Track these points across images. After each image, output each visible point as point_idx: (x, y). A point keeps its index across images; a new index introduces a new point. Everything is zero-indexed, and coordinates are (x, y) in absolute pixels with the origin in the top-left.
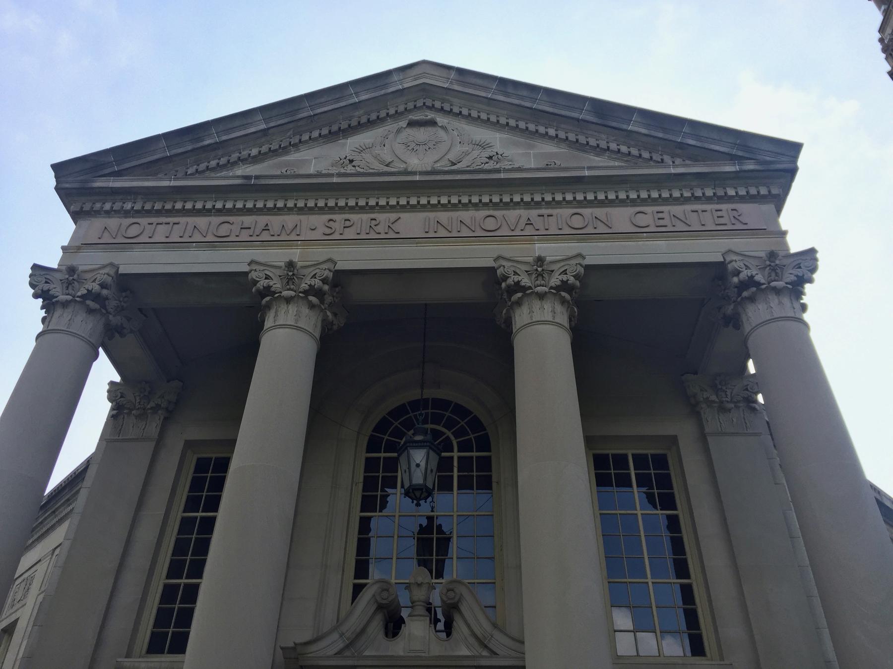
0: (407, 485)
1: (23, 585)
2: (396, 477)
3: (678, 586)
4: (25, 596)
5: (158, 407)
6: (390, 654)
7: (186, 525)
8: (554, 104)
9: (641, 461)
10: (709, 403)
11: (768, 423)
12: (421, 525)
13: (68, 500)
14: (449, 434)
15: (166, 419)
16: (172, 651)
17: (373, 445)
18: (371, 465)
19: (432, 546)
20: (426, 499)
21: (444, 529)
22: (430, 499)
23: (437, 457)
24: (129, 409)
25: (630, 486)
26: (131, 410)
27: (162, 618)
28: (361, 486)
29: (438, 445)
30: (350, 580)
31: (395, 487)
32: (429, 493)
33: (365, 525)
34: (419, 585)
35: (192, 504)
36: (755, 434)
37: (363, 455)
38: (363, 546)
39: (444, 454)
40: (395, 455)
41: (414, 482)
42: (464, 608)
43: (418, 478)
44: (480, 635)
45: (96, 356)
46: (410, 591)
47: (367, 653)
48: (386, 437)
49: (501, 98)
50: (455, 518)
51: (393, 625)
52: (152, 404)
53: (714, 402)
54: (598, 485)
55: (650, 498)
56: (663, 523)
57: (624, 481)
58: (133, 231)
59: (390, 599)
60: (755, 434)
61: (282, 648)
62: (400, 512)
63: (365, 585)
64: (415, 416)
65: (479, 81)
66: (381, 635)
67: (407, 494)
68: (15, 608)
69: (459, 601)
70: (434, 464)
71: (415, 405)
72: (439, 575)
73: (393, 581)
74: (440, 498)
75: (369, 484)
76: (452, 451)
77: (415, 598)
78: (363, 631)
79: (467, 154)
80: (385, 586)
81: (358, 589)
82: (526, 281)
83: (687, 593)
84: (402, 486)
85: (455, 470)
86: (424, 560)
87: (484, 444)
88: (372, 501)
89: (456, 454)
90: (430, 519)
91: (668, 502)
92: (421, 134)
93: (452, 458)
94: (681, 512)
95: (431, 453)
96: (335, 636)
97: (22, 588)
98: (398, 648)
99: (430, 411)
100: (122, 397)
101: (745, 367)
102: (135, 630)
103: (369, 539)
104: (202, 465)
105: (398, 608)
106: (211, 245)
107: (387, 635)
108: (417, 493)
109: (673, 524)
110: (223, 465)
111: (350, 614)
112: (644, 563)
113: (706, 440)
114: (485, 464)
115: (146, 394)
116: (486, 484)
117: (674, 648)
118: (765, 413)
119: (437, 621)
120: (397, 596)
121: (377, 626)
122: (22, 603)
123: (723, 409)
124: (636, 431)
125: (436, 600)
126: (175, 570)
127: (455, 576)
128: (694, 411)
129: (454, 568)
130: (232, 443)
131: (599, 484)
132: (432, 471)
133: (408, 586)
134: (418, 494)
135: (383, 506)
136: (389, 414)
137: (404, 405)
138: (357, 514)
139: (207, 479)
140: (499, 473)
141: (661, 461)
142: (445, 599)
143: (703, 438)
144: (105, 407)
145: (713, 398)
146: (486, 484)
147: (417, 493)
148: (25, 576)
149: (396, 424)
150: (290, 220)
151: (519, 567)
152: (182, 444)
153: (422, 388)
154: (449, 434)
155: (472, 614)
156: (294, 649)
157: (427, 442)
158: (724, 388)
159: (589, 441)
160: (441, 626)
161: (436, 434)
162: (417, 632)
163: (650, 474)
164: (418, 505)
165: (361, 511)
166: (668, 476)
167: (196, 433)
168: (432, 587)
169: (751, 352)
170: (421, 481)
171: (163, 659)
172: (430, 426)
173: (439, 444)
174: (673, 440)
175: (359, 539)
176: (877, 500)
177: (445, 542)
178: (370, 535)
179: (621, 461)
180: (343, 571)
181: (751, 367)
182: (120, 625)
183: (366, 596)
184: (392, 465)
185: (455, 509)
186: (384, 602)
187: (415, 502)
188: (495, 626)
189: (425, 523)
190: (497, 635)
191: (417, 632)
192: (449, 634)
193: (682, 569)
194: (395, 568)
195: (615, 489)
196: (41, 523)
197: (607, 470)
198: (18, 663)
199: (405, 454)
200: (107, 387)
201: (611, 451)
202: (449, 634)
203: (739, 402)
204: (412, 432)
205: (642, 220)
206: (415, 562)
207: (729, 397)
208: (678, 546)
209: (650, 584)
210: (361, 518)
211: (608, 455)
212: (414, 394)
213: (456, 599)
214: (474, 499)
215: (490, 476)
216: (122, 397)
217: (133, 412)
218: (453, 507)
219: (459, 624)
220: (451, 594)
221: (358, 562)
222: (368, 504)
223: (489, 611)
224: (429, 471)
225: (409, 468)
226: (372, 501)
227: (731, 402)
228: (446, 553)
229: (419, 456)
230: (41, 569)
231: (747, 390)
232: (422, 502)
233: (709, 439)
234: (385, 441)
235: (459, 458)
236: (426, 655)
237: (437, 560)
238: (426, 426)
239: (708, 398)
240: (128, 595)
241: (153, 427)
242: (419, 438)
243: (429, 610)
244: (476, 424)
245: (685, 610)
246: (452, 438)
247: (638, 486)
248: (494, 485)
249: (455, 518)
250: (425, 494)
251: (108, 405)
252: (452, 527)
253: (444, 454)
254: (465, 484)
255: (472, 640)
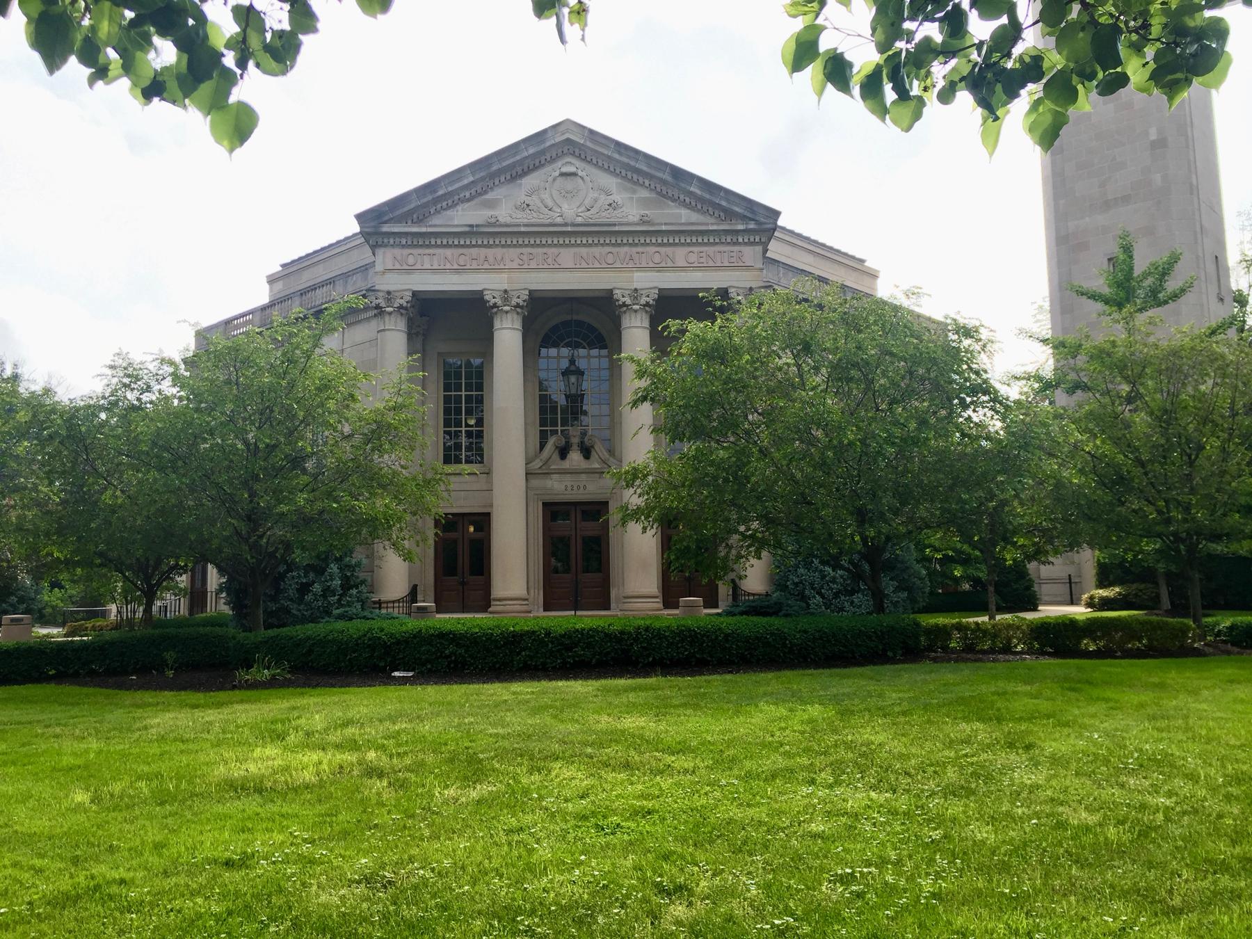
8: (649, 166)
49: (616, 156)
58: (411, 260)
65: (603, 141)
71: (566, 324)
79: (596, 200)
82: (628, 301)
92: (569, 184)
106: (457, 271)
121: (556, 456)
150: (499, 252)
155: (600, 450)
205: (693, 258)
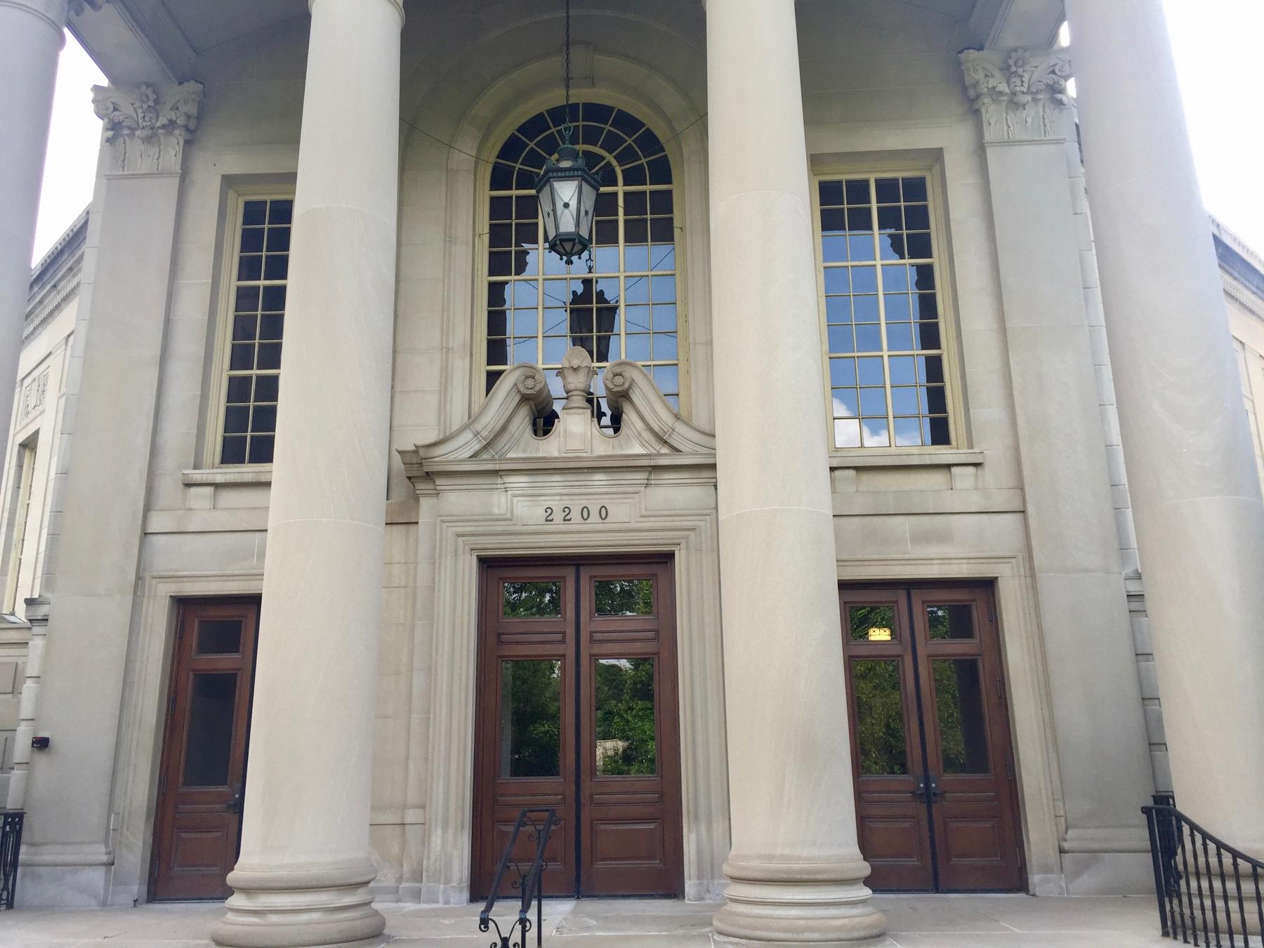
0: (551, 235)
1: (35, 385)
2: (537, 224)
3: (923, 361)
4: (41, 401)
5: (172, 124)
6: (541, 455)
7: (245, 298)
9: (887, 189)
10: (995, 94)
11: (1077, 126)
12: (574, 293)
13: (70, 269)
14: (610, 158)
15: (187, 142)
16: (255, 459)
17: (499, 179)
18: (498, 208)
19: (591, 318)
20: (579, 254)
21: (607, 296)
22: (585, 255)
23: (594, 193)
24: (129, 128)
25: (870, 228)
26: (132, 130)
27: (234, 419)
28: (486, 239)
29: (594, 174)
30: (482, 367)
31: (536, 242)
32: (584, 245)
33: (496, 293)
34: (576, 370)
35: (248, 268)
36: (1058, 142)
37: (486, 194)
38: (496, 322)
39: (602, 189)
40: (533, 192)
41: (563, 229)
42: (636, 397)
43: (567, 225)
44: (656, 428)
45: (61, 41)
46: (564, 378)
47: (511, 455)
48: (518, 166)
50: (622, 279)
51: (544, 421)
52: (163, 120)
53: (1001, 93)
54: (824, 229)
55: (896, 246)
56: (911, 276)
57: (861, 222)
59: (537, 388)
60: (1058, 142)
61: (399, 452)
62: (545, 279)
63: (500, 373)
64: (559, 132)
66: (529, 431)
67: (553, 248)
68: (31, 416)
69: (630, 387)
70: (589, 203)
71: (557, 114)
72: (603, 357)
73: (540, 366)
74: (601, 254)
75: (498, 235)
76: (616, 185)
77: (571, 386)
78: (504, 428)
80: (530, 373)
81: (492, 378)
83: (934, 368)
84: (546, 239)
85: (621, 211)
86: (582, 338)
87: (662, 172)
88: (504, 259)
89: (621, 189)
90: (587, 283)
91: (921, 246)
93: (616, 194)
94: (937, 260)
95: (585, 186)
96: (468, 435)
97: (34, 392)
98: (551, 447)
99: (581, 123)
100: (115, 109)
101: (1053, 36)
102: (204, 397)
103: (504, 313)
104: (253, 212)
105: (549, 400)
107: (535, 433)
108: (567, 246)
109: (925, 277)
110: (283, 211)
111: (484, 408)
112: (877, 300)
113: (984, 152)
114: (664, 202)
115: (151, 103)
116: (665, 233)
117: (912, 443)
118: (1075, 111)
119: (600, 415)
120: (546, 385)
121: (522, 422)
122: (38, 409)
123: (1014, 104)
124: (887, 142)
125: (599, 389)
126: (240, 358)
127: (623, 357)
128: (973, 110)
129: (620, 346)
130: (291, 178)
131: (825, 227)
132: (587, 213)
133: (560, 372)
134: (568, 246)
135: (521, 268)
136: (520, 129)
137: (541, 115)
138: (484, 279)
139: (265, 234)
140: (683, 215)
141: (916, 188)
142: (611, 386)
143: (980, 150)
144: (96, 128)
145: (1003, 87)
146: (665, 233)
147: (567, 246)
148: (35, 374)
149: (532, 145)
151: (709, 343)
152: (218, 181)
153: (568, 87)
154: (610, 158)
155: (647, 404)
156: (416, 452)
157: (577, 170)
158: (1020, 71)
159: (815, 161)
160: (606, 421)
161: (592, 159)
162: (576, 431)
163: (899, 208)
164: (569, 262)
165: (490, 275)
166: (927, 237)
167: (236, 165)
168: (592, 373)
169: (1068, 15)
170: (572, 229)
171: (244, 470)
172: (581, 147)
173: (596, 173)
174: (936, 156)
175: (490, 313)
176: (1215, 237)
177: (608, 314)
178: (506, 306)
179: (858, 190)
180: (471, 354)
181: (1065, 36)
182: (178, 430)
183: (504, 386)
184: (529, 207)
185: (622, 269)
186: (529, 392)
187: (565, 258)
188: (677, 417)
189: (580, 289)
190: (680, 428)
191: (576, 431)
192: (616, 430)
193: (930, 337)
194: (543, 347)
195: (847, 232)
196: (40, 302)
197: (839, 206)
198: (41, 557)
199: (547, 189)
200: (91, 95)
201: (844, 175)
202: (616, 430)
203: (1038, 92)
204: (556, 156)
206: (569, 341)
207: (1026, 85)
208: (928, 306)
209: (886, 358)
210: (491, 284)
211: (840, 182)
212: (556, 97)
213: (626, 386)
214: (649, 252)
215: (671, 219)
216: (115, 109)
217: (138, 133)
218: (615, 265)
219: (629, 416)
220: (619, 380)
221: (491, 344)
222: (499, 264)
223: (671, 400)
224: (582, 213)
225: (554, 210)
226: (504, 259)
227: (1028, 92)
228: (611, 328)
229: (567, 191)
230: (55, 364)
231: (1053, 72)
232: (575, 258)
233: (989, 150)
234: (517, 171)
235: (625, 194)
236: (589, 455)
237: (598, 338)
238: (577, 147)
239: (994, 88)
240: (182, 390)
241: (171, 154)
242: (566, 164)
243: (590, 401)
244: (650, 142)
245: (929, 390)
246: (615, 163)
247: (880, 228)
248: (677, 232)
249: (622, 279)
250: (578, 247)
251: (99, 124)
252: (617, 292)
253: (602, 189)
254: (635, 236)
255: (647, 435)
